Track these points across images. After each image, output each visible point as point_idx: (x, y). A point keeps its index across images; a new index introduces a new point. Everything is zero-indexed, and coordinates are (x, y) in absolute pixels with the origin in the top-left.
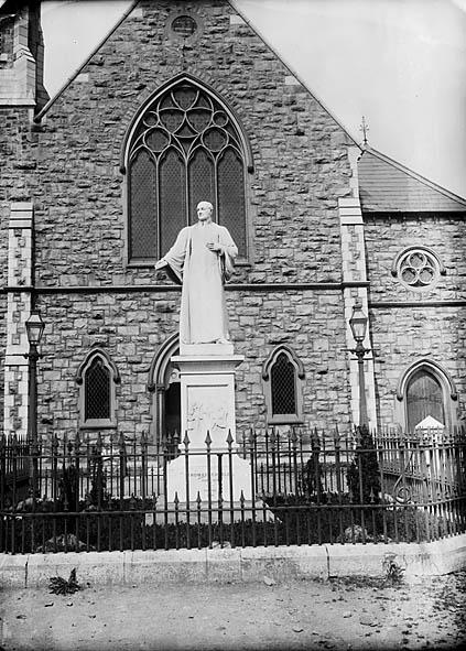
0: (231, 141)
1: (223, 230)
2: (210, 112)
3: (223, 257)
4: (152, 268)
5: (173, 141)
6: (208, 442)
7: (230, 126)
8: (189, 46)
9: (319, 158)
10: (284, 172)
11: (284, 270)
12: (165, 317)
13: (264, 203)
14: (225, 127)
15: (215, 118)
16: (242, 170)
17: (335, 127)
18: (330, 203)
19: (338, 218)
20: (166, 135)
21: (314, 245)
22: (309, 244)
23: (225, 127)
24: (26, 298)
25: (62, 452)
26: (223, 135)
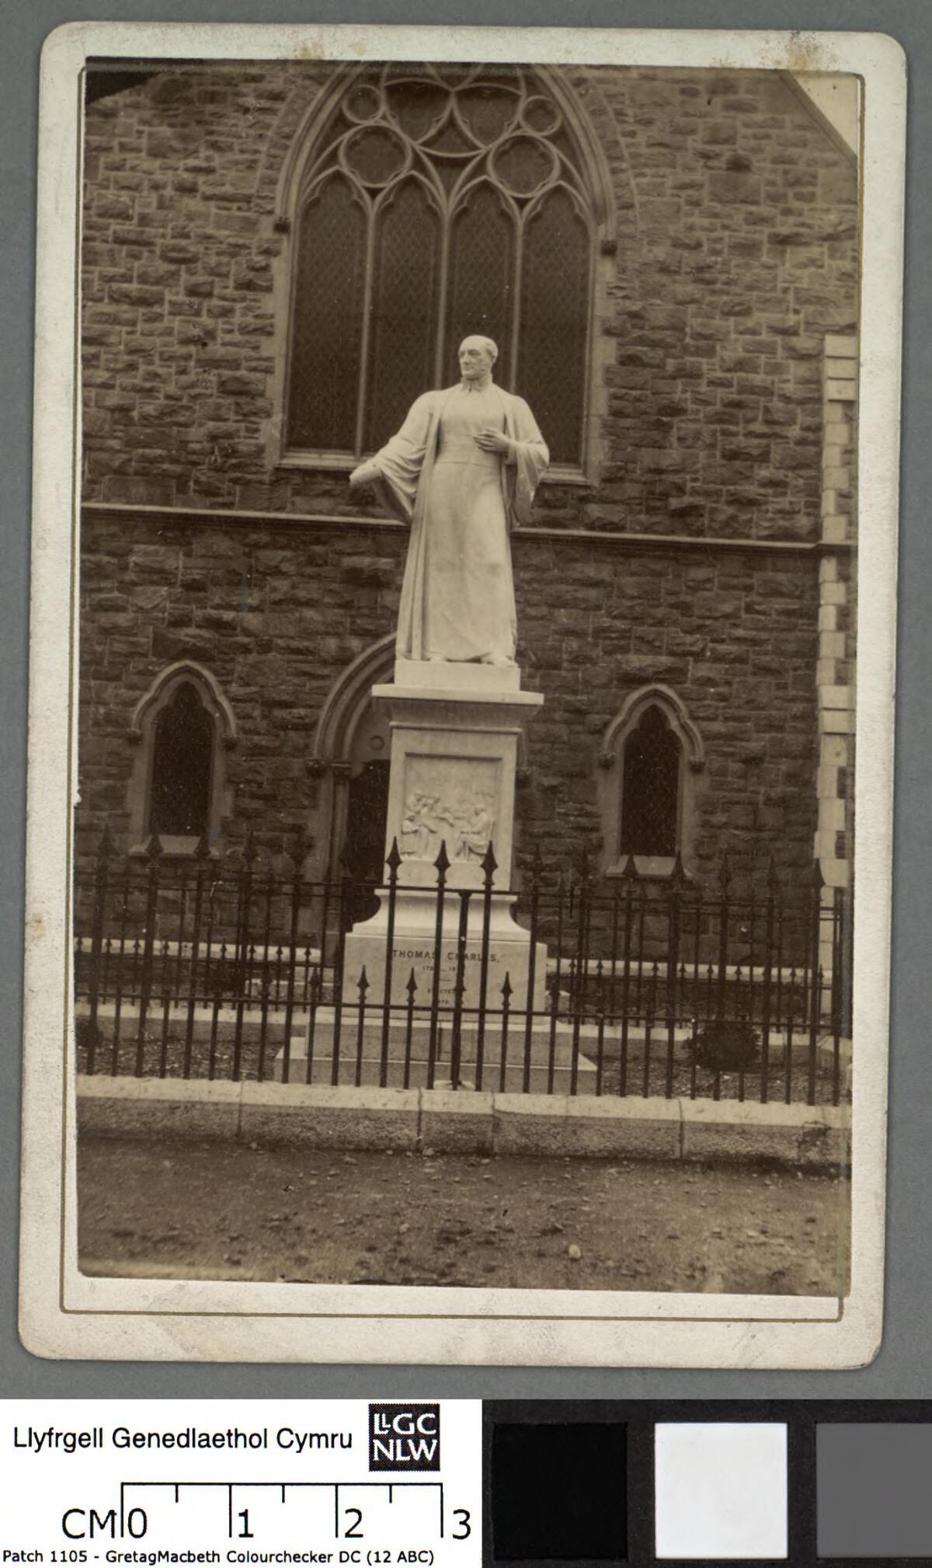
0: (565, 174)
1: (518, 408)
2: (515, 99)
3: (512, 469)
4: (343, 475)
5: (418, 164)
6: (442, 864)
7: (562, 137)
8: (235, 1235)
9: (784, 230)
10: (689, 259)
11: (675, 503)
12: (363, 597)
13: (637, 333)
14: (551, 138)
15: (528, 114)
16: (586, 247)
17: (831, 156)
18: (803, 343)
19: (819, 382)
20: (399, 147)
21: (753, 445)
22: (741, 441)
23: (551, 138)
24: (367, 1011)
25: (616, 987)
26: (546, 157)
